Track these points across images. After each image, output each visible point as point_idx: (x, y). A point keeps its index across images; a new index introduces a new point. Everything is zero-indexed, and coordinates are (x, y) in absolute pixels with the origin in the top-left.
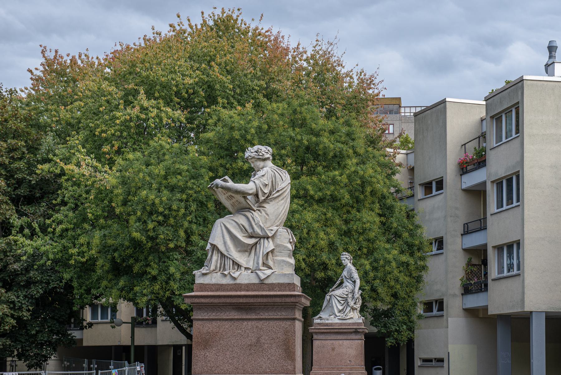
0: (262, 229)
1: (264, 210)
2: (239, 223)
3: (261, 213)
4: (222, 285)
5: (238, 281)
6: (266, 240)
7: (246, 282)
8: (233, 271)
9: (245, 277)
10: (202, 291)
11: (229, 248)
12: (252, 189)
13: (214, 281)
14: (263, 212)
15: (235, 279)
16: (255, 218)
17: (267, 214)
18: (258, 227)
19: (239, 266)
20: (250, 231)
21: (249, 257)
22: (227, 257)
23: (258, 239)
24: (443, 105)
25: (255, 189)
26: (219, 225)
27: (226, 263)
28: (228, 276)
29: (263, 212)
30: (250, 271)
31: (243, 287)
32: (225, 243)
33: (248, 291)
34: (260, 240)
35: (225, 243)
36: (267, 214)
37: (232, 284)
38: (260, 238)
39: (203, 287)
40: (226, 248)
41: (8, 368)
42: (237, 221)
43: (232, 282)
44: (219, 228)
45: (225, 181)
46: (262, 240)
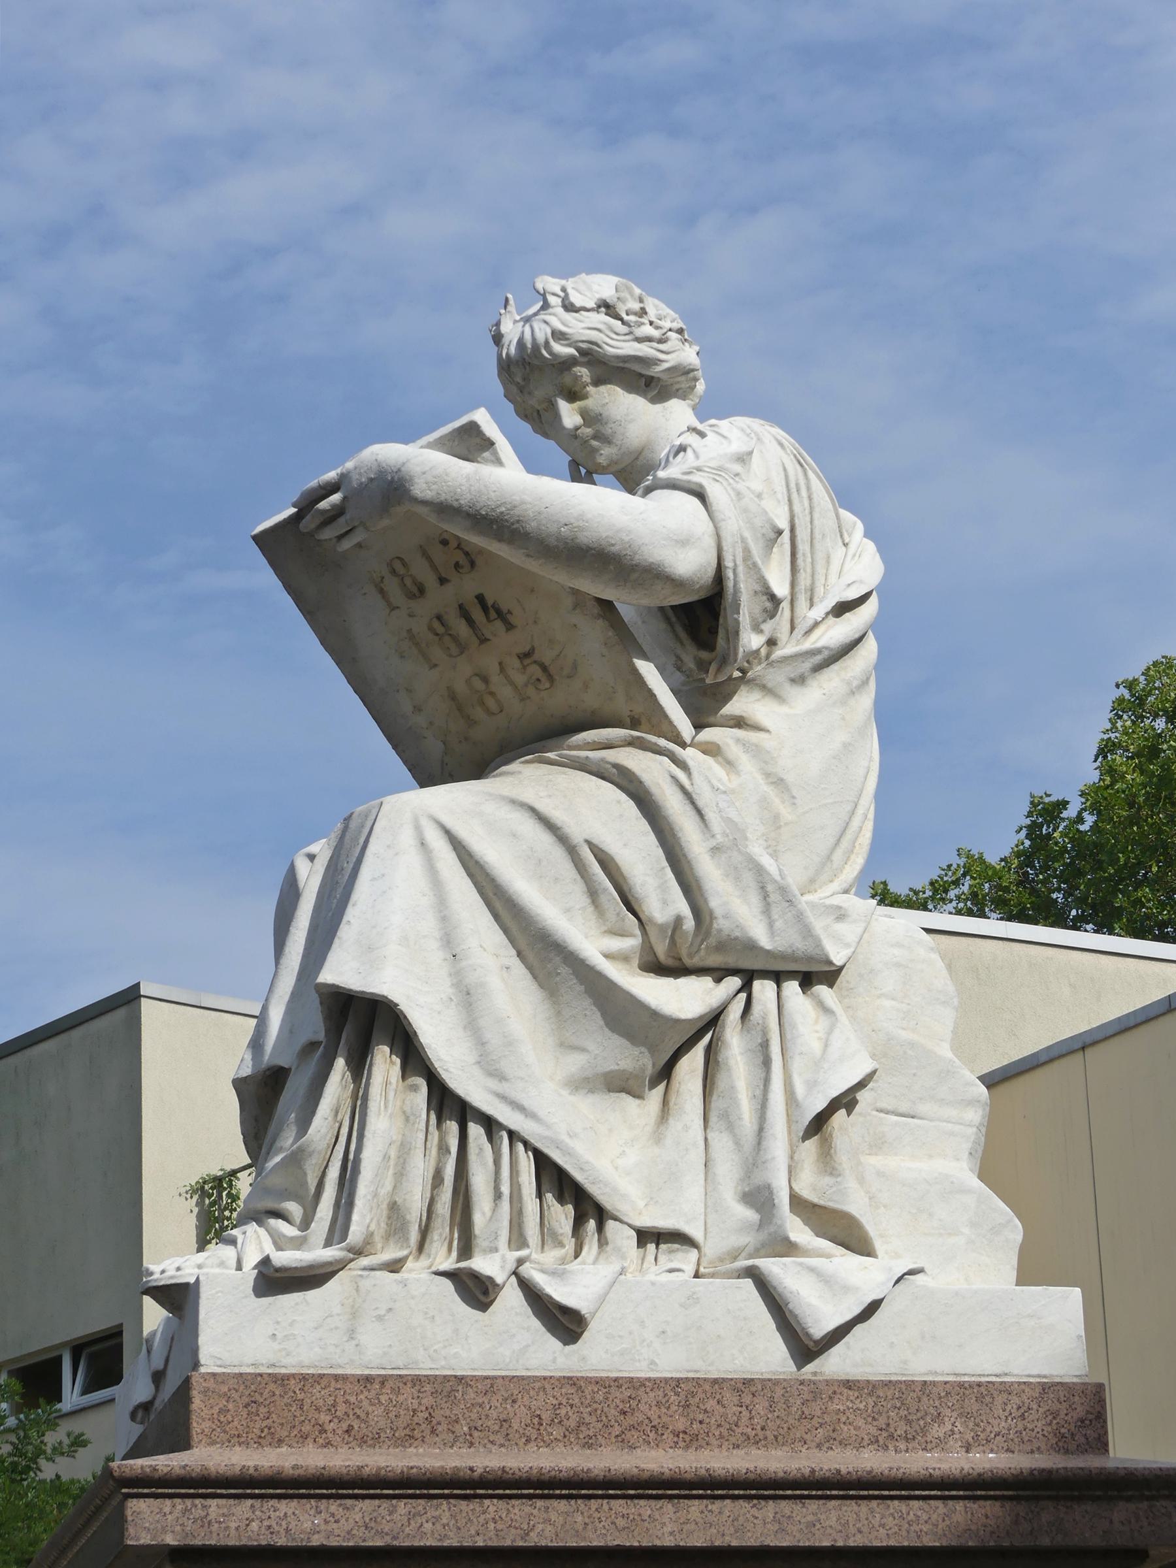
0: (771, 893)
1: (756, 751)
2: (577, 833)
3: (729, 764)
4: (452, 1386)
5: (593, 1356)
6: (792, 987)
7: (668, 1360)
8: (551, 1256)
9: (660, 1322)
10: (269, 1438)
11: (510, 1043)
12: (684, 542)
13: (376, 1350)
14: (745, 762)
15: (565, 1323)
16: (705, 798)
17: (779, 782)
18: (733, 874)
19: (588, 1209)
20: (664, 902)
21: (657, 1137)
22: (490, 1125)
23: (735, 982)
24: (120, 1014)
25: (710, 543)
26: (407, 838)
27: (480, 1180)
28: (511, 1299)
29: (745, 762)
30: (687, 1260)
31: (647, 1408)
32: (467, 997)
33: (690, 1440)
34: (747, 987)
35: (467, 997)
36: (779, 782)
37: (544, 1383)
38: (748, 969)
39: (272, 1397)
40: (481, 1043)
41: (640, 492)
42: (557, 815)
43: (544, 1355)
44: (410, 863)
45: (470, 443)
46: (764, 989)
